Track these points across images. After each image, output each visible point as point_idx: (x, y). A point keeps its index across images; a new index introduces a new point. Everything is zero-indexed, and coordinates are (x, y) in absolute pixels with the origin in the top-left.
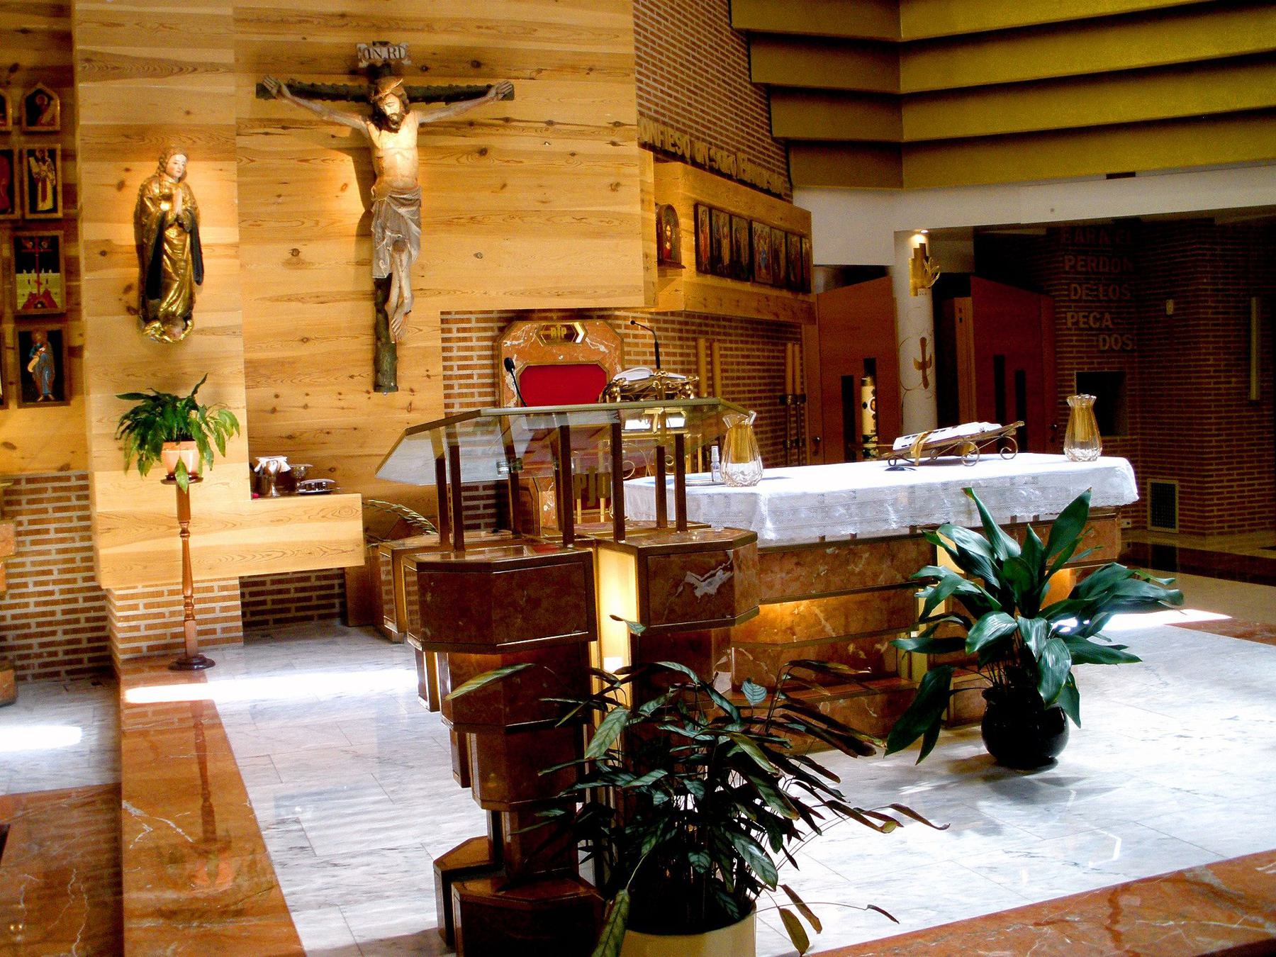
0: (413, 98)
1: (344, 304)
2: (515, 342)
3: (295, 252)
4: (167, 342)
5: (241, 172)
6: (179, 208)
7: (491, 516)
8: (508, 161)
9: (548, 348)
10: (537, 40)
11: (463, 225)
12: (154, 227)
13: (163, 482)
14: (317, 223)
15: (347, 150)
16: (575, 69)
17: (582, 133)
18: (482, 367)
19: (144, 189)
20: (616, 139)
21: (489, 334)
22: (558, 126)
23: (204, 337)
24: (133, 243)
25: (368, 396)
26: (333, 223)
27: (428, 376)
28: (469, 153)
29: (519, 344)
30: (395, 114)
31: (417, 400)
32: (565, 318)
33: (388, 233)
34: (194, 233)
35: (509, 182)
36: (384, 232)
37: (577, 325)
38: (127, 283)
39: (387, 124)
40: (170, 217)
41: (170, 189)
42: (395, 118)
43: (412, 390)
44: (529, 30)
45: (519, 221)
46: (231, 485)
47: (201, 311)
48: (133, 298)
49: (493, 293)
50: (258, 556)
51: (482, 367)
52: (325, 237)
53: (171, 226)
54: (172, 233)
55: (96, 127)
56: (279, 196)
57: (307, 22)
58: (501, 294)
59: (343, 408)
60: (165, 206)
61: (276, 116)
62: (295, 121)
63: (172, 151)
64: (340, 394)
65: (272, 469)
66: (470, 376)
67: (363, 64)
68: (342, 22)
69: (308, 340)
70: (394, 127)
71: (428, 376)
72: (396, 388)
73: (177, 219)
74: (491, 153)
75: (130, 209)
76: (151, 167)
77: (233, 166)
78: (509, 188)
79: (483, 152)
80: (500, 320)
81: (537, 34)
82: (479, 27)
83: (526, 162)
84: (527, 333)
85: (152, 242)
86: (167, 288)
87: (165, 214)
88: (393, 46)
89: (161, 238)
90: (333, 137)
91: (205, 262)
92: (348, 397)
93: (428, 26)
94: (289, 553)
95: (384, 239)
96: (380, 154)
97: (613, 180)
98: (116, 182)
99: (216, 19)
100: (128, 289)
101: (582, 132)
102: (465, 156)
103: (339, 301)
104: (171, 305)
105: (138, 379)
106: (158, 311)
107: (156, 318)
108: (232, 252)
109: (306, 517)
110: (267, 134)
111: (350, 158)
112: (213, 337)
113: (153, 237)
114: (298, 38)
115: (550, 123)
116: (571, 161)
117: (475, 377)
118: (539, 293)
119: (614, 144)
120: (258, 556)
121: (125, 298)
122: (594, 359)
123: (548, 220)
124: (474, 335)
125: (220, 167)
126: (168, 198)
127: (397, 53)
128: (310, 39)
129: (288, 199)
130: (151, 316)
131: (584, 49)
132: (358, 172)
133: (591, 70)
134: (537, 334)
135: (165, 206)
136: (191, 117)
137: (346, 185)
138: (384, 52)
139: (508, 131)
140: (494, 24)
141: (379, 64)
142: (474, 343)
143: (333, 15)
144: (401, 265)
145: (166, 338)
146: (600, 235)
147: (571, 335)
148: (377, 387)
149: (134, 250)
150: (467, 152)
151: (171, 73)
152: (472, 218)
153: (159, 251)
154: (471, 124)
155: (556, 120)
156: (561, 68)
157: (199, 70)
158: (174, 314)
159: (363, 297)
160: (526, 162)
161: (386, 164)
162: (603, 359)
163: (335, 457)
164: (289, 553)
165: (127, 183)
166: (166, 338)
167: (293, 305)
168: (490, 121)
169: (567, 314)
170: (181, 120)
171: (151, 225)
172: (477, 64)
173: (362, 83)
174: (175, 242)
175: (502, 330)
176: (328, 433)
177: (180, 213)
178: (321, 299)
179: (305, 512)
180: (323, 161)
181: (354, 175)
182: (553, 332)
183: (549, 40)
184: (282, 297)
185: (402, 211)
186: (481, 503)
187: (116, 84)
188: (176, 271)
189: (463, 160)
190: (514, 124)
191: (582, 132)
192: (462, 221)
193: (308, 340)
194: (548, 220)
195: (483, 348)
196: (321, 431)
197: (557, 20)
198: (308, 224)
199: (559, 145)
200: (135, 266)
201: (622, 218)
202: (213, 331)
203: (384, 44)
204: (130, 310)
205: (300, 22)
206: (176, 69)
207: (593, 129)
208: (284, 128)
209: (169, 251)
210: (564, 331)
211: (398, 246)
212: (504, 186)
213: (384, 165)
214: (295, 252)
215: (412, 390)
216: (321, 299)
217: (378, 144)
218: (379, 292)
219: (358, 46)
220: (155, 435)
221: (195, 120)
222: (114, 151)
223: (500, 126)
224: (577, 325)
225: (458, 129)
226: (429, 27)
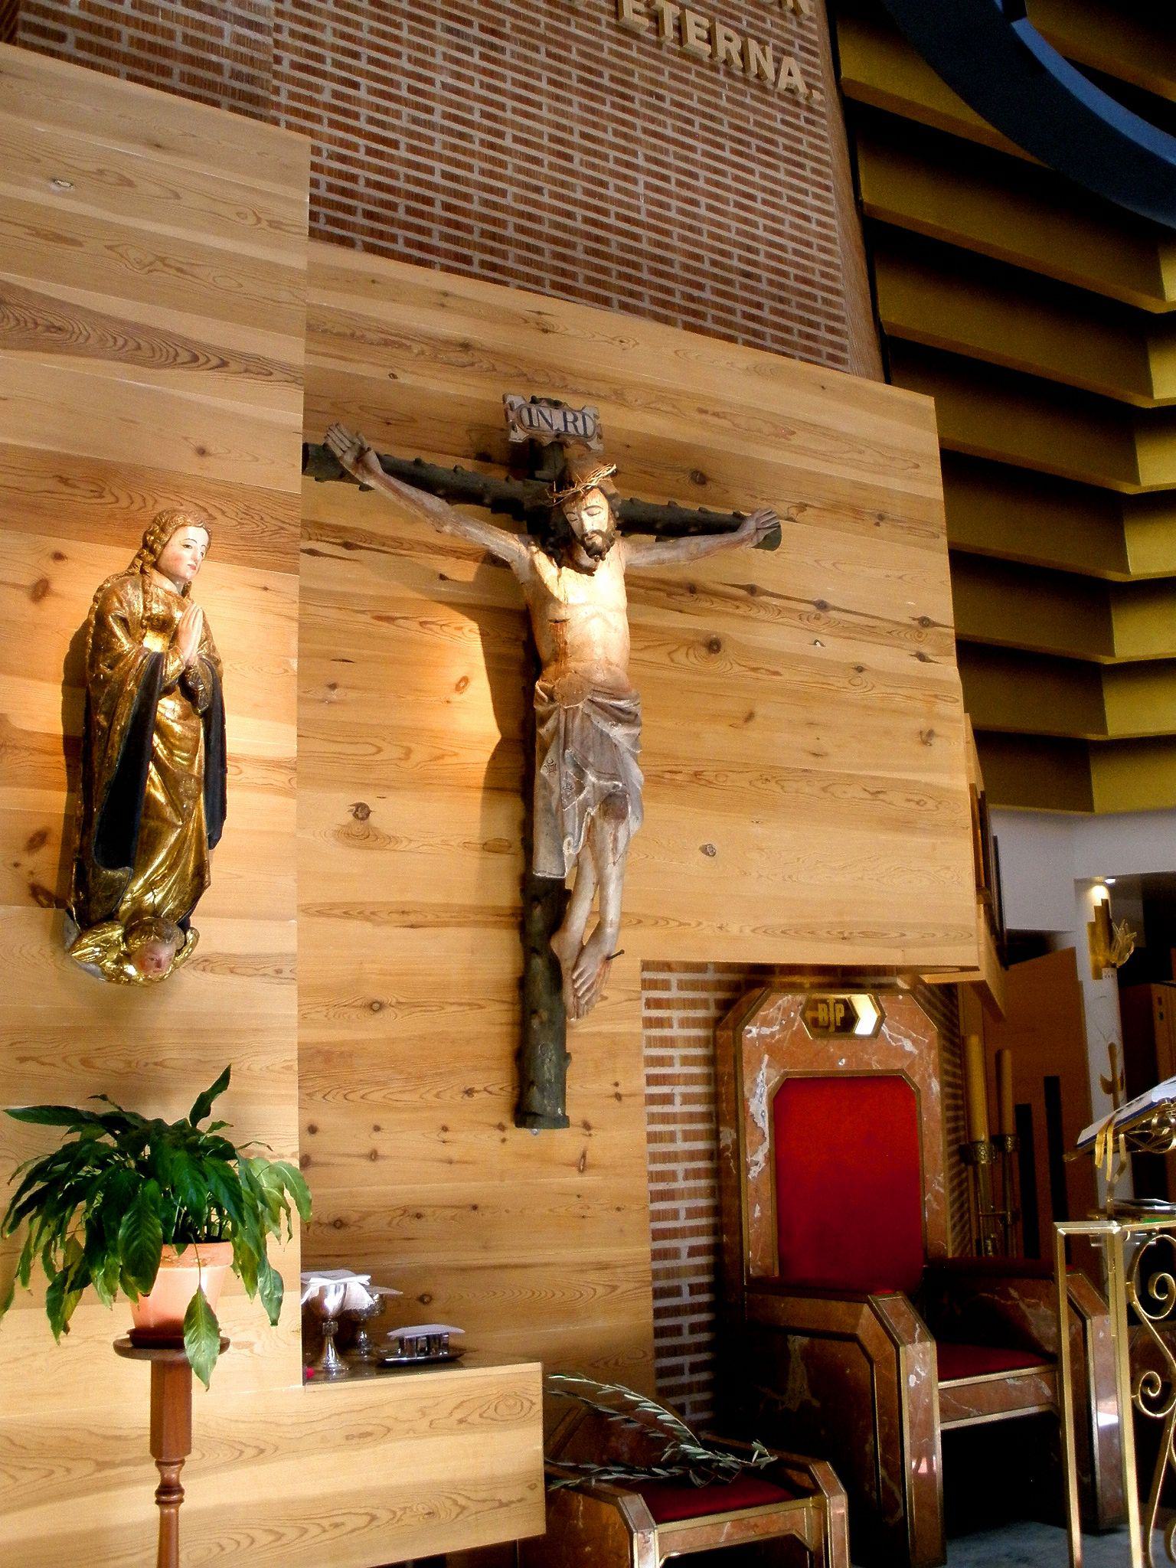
0: (629, 523)
1: (451, 932)
2: (766, 1031)
3: (361, 812)
4: (130, 980)
5: (307, 594)
6: (190, 650)
7: (702, 1387)
8: (755, 670)
9: (821, 1043)
10: (803, 451)
11: (679, 787)
12: (131, 686)
13: (121, 1349)
14: (409, 752)
15: (469, 610)
16: (857, 512)
17: (871, 630)
18: (690, 1079)
19: (103, 599)
20: (926, 650)
21: (700, 1013)
22: (833, 614)
23: (210, 977)
24: (60, 730)
25: (502, 1135)
26: (442, 757)
27: (618, 1096)
28: (690, 645)
29: (772, 1035)
30: (599, 532)
31: (599, 1145)
32: (831, 987)
33: (591, 778)
34: (213, 718)
35: (760, 710)
36: (580, 773)
37: (864, 1006)
38: (37, 826)
39: (571, 556)
40: (172, 668)
41: (168, 605)
42: (598, 540)
43: (587, 1126)
44: (783, 431)
45: (778, 789)
46: (257, 1349)
47: (207, 914)
48: (46, 864)
49: (734, 929)
50: (314, 1530)
51: (690, 1079)
52: (423, 783)
53: (168, 692)
54: (169, 708)
55: (40, 455)
56: (333, 687)
57: (401, 346)
58: (747, 931)
59: (450, 1162)
60: (154, 643)
61: (333, 521)
62: (371, 536)
63: (180, 520)
64: (445, 1129)
65: (332, 1304)
66: (667, 1099)
67: (518, 436)
68: (465, 358)
69: (382, 1006)
70: (586, 560)
71: (618, 1096)
72: (562, 1122)
73: (183, 679)
74: (727, 648)
75: (55, 652)
76: (121, 557)
77: (288, 585)
78: (758, 719)
79: (714, 646)
80: (719, 985)
81: (795, 440)
82: (702, 411)
83: (787, 675)
84: (786, 1012)
85: (123, 722)
86: (151, 850)
87: (157, 662)
88: (571, 410)
89: (144, 721)
90: (442, 577)
91: (233, 797)
92: (462, 1136)
93: (615, 392)
94: (384, 1515)
95: (580, 788)
96: (562, 614)
97: (922, 724)
98: (28, 579)
99: (273, 270)
100: (37, 840)
101: (871, 629)
102: (683, 650)
103: (446, 924)
104: (150, 886)
105: (46, 1069)
106: (120, 899)
107: (111, 917)
108: (280, 778)
109: (425, 1422)
110: (312, 552)
111: (475, 626)
112: (231, 979)
113: (125, 713)
114: (380, 373)
115: (822, 606)
116: (857, 681)
117: (678, 1100)
118: (811, 933)
119: (922, 657)
120: (314, 1530)
121: (29, 861)
122: (897, 1065)
123: (824, 789)
124: (676, 1014)
125: (263, 583)
126: (164, 626)
127: (579, 424)
128: (405, 379)
129: (352, 695)
130: (98, 911)
131: (868, 479)
132: (488, 655)
133: (881, 518)
134: (803, 1014)
135: (154, 643)
136: (208, 461)
137: (465, 680)
138: (557, 420)
139: (753, 613)
140: (728, 410)
141: (547, 441)
142: (676, 1032)
143: (448, 343)
144: (615, 848)
145: (130, 969)
146: (904, 824)
147: (850, 1019)
148: (524, 1114)
149: (60, 747)
150: (689, 643)
151: (173, 362)
152: (696, 774)
153: (137, 751)
154: (692, 589)
155: (831, 601)
156: (834, 508)
157: (233, 366)
158: (155, 911)
159: (481, 916)
160: (787, 675)
161: (570, 636)
162: (911, 1066)
163: (428, 1270)
164: (384, 1515)
165: (55, 586)
166: (130, 969)
167: (355, 928)
168: (721, 588)
169: (858, 980)
170: (188, 465)
171: (123, 683)
172: (700, 479)
173: (497, 478)
174: (177, 728)
175: (725, 1006)
176: (419, 1216)
177: (195, 662)
178: (410, 917)
179: (423, 1413)
180: (422, 624)
181: (481, 662)
182: (822, 1014)
183: (815, 454)
184: (333, 906)
185: (619, 733)
186: (686, 1360)
187: (54, 363)
188: (172, 802)
189: (680, 657)
190: (764, 598)
191: (871, 629)
192: (678, 777)
193: (382, 1006)
194: (824, 789)
195: (690, 1042)
196: (405, 1211)
197: (825, 419)
198: (391, 752)
199: (835, 649)
200: (54, 786)
201: (940, 796)
202: (231, 965)
203: (556, 405)
204: (36, 892)
205: (386, 343)
206: (184, 356)
207: (889, 627)
208: (347, 546)
209: (161, 750)
210: (841, 1014)
211: (613, 805)
212: (750, 717)
213: (569, 637)
214: (361, 812)
215: (587, 1126)
216: (410, 917)
217: (557, 592)
218: (538, 912)
219: (510, 399)
220: (136, 1227)
221: (217, 470)
222: (35, 508)
223: (735, 598)
224: (864, 1006)
225: (670, 595)
226: (618, 396)
